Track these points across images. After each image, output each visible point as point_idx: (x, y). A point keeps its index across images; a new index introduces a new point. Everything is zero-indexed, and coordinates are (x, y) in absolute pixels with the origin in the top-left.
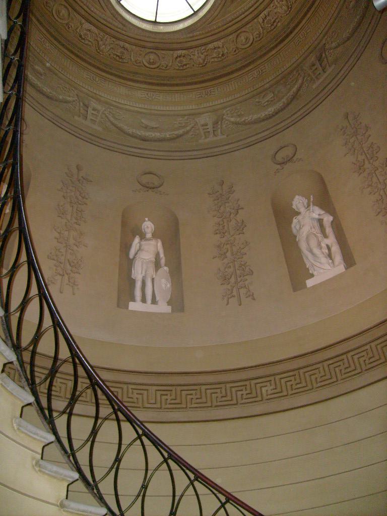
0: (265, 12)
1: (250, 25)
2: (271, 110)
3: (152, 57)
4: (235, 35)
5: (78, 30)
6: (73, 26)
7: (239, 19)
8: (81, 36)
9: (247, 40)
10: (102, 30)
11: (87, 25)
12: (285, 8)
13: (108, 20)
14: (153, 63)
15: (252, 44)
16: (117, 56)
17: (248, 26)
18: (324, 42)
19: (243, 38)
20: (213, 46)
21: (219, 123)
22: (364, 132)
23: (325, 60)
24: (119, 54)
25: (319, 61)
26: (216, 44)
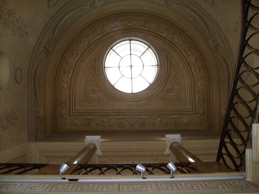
0: (78, 58)
1: (84, 50)
2: (66, 18)
3: (130, 25)
4: (90, 43)
5: (168, 33)
6: (171, 34)
7: (90, 52)
8: (167, 30)
9: (84, 43)
10: (156, 34)
11: (164, 35)
12: (69, 62)
13: (154, 39)
14: (129, 22)
15: (81, 42)
16: (148, 23)
17: (85, 49)
18: (48, 58)
19: (86, 43)
20: (100, 36)
21: (92, 4)
22: (15, 32)
23: (45, 52)
24: (147, 23)
25: (48, 49)
26: (99, 37)
